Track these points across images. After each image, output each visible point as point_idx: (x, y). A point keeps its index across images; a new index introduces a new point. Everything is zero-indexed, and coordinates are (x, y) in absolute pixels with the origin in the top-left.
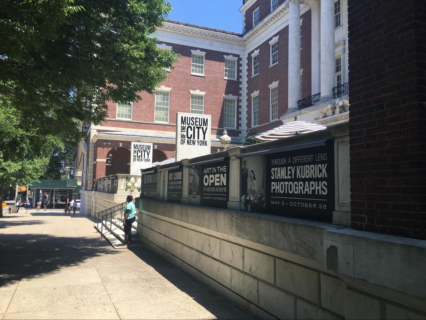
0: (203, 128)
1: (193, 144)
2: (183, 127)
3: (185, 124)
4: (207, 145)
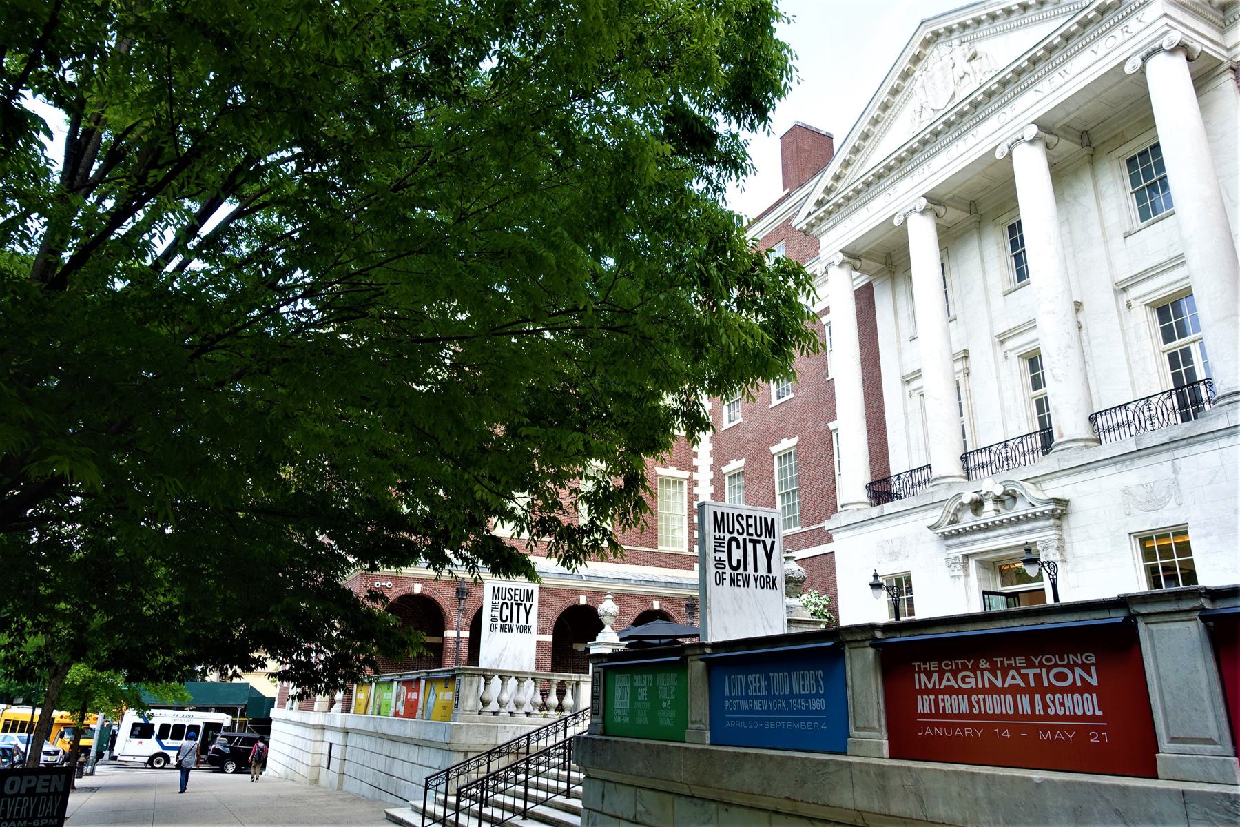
0: (764, 542)
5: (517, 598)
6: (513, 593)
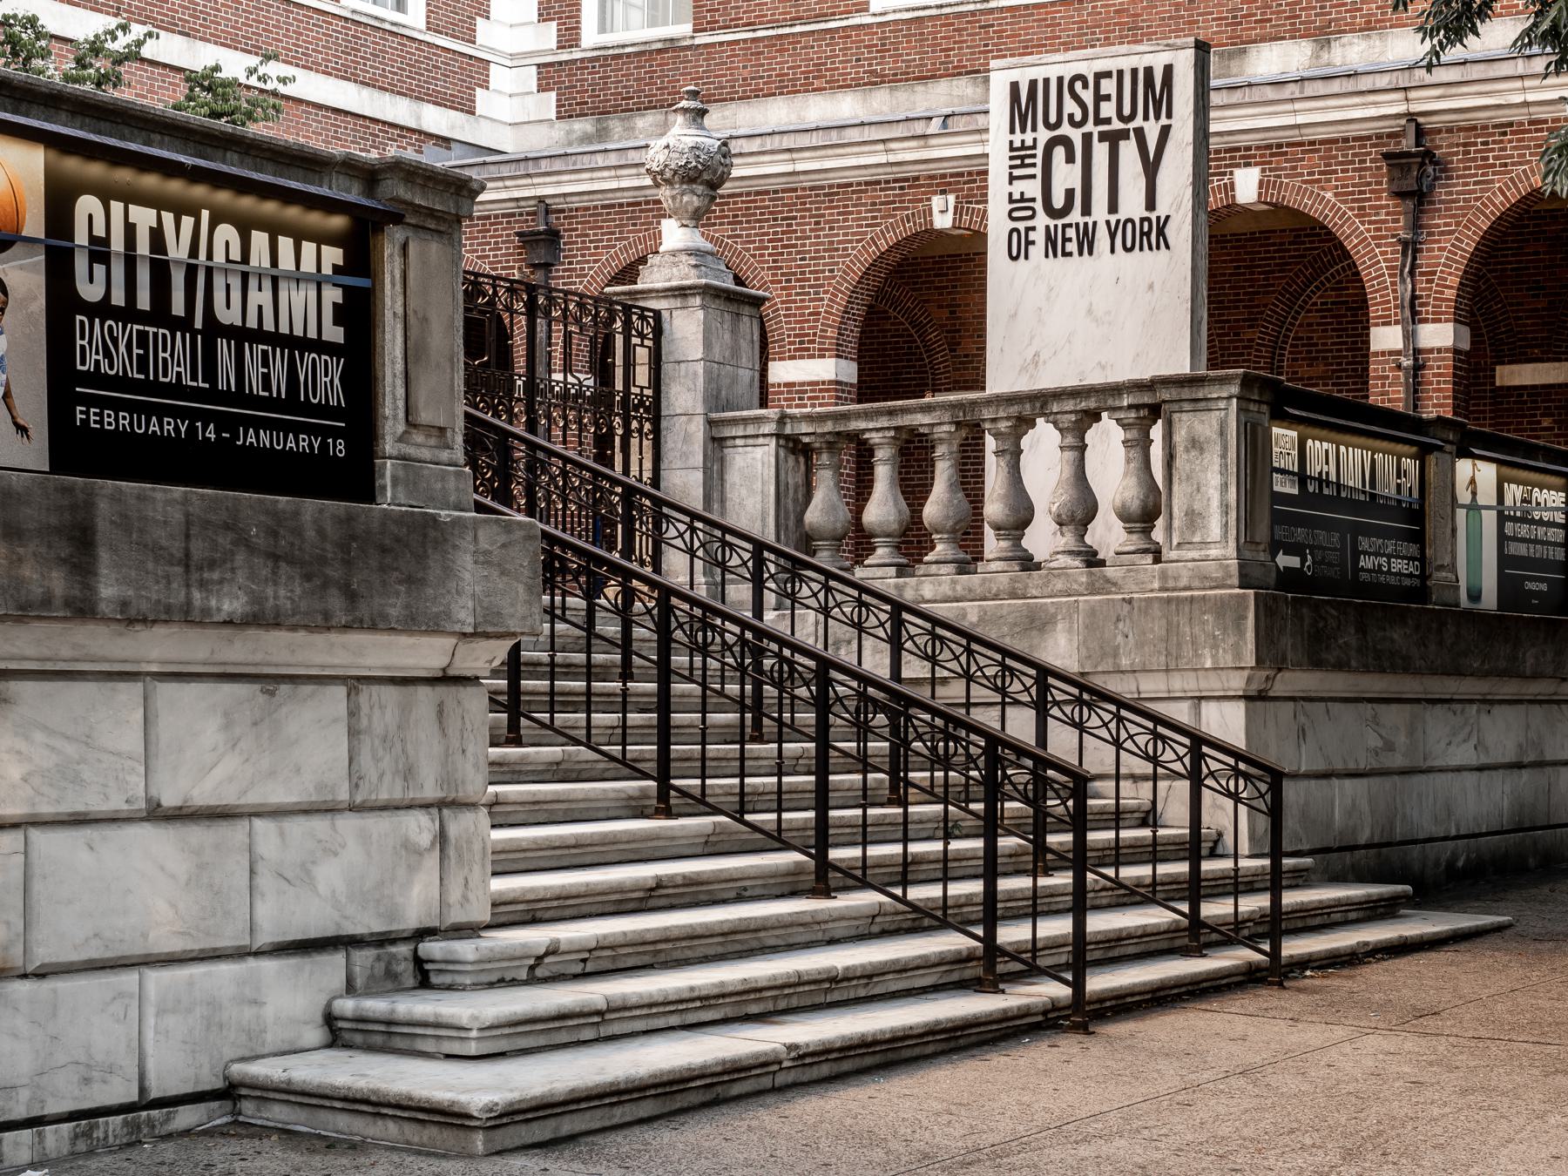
0: (1140, 133)
1: (1081, 254)
2: (1023, 147)
3: (1034, 129)
4: (1167, 247)
5: (1108, 109)
6: (1088, 96)
